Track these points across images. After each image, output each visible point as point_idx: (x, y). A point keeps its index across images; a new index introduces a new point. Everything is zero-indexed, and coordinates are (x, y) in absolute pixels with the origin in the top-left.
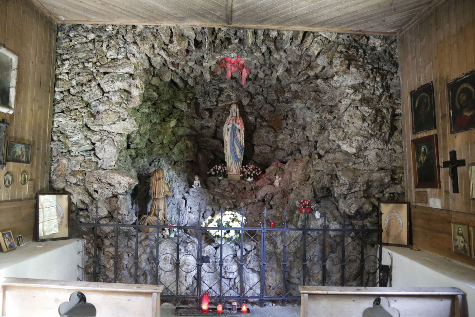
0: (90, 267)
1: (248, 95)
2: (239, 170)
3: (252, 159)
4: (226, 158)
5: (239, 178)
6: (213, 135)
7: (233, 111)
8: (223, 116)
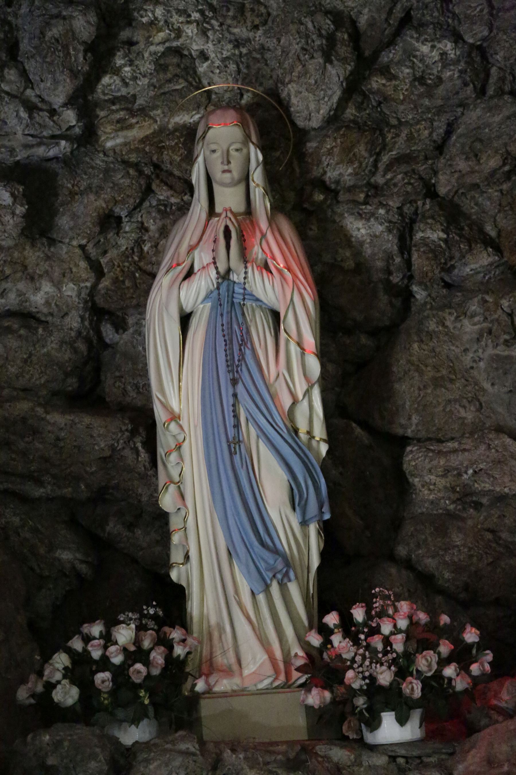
0: (484, 495)
1: (331, 39)
2: (297, 650)
3: (392, 558)
4: (176, 556)
5: (301, 721)
6: (72, 383)
7: (217, 175)
8: (143, 228)
